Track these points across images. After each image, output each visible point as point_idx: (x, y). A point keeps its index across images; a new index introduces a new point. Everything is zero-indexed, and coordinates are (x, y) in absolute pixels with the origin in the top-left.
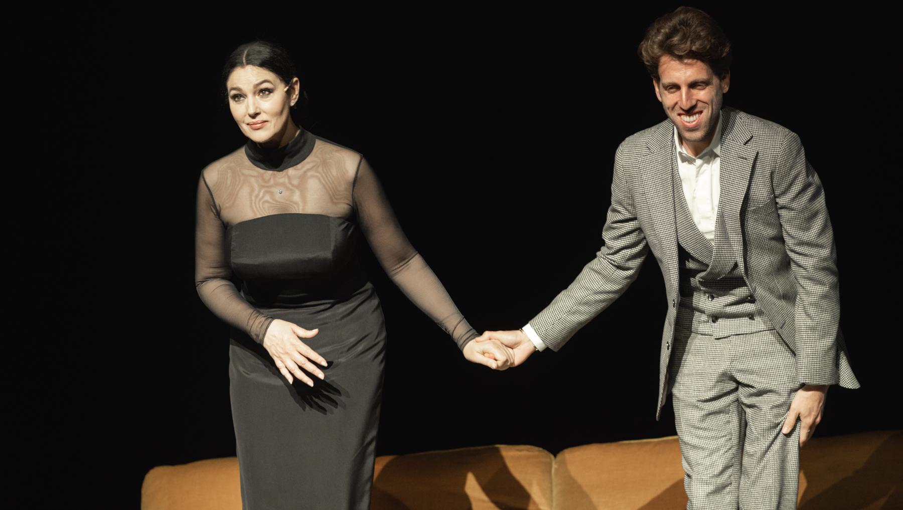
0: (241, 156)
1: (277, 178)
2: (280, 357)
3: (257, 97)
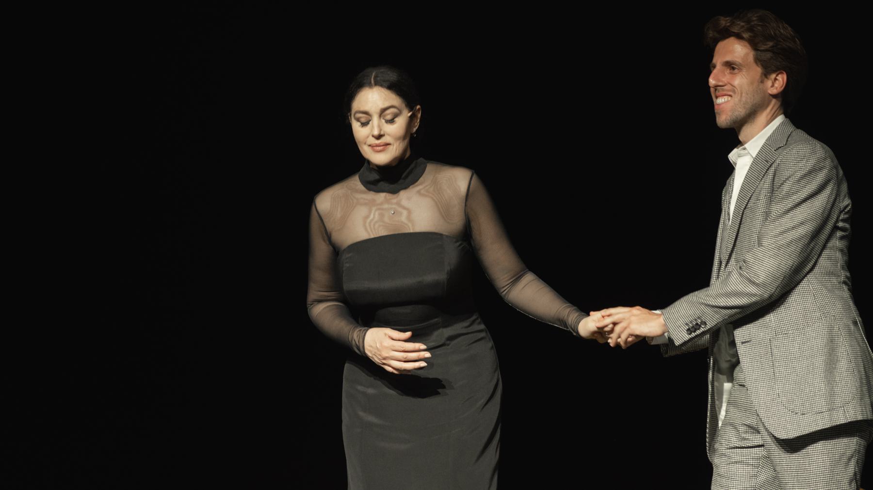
0: (355, 182)
1: (393, 200)
2: (384, 364)
3: (378, 118)
